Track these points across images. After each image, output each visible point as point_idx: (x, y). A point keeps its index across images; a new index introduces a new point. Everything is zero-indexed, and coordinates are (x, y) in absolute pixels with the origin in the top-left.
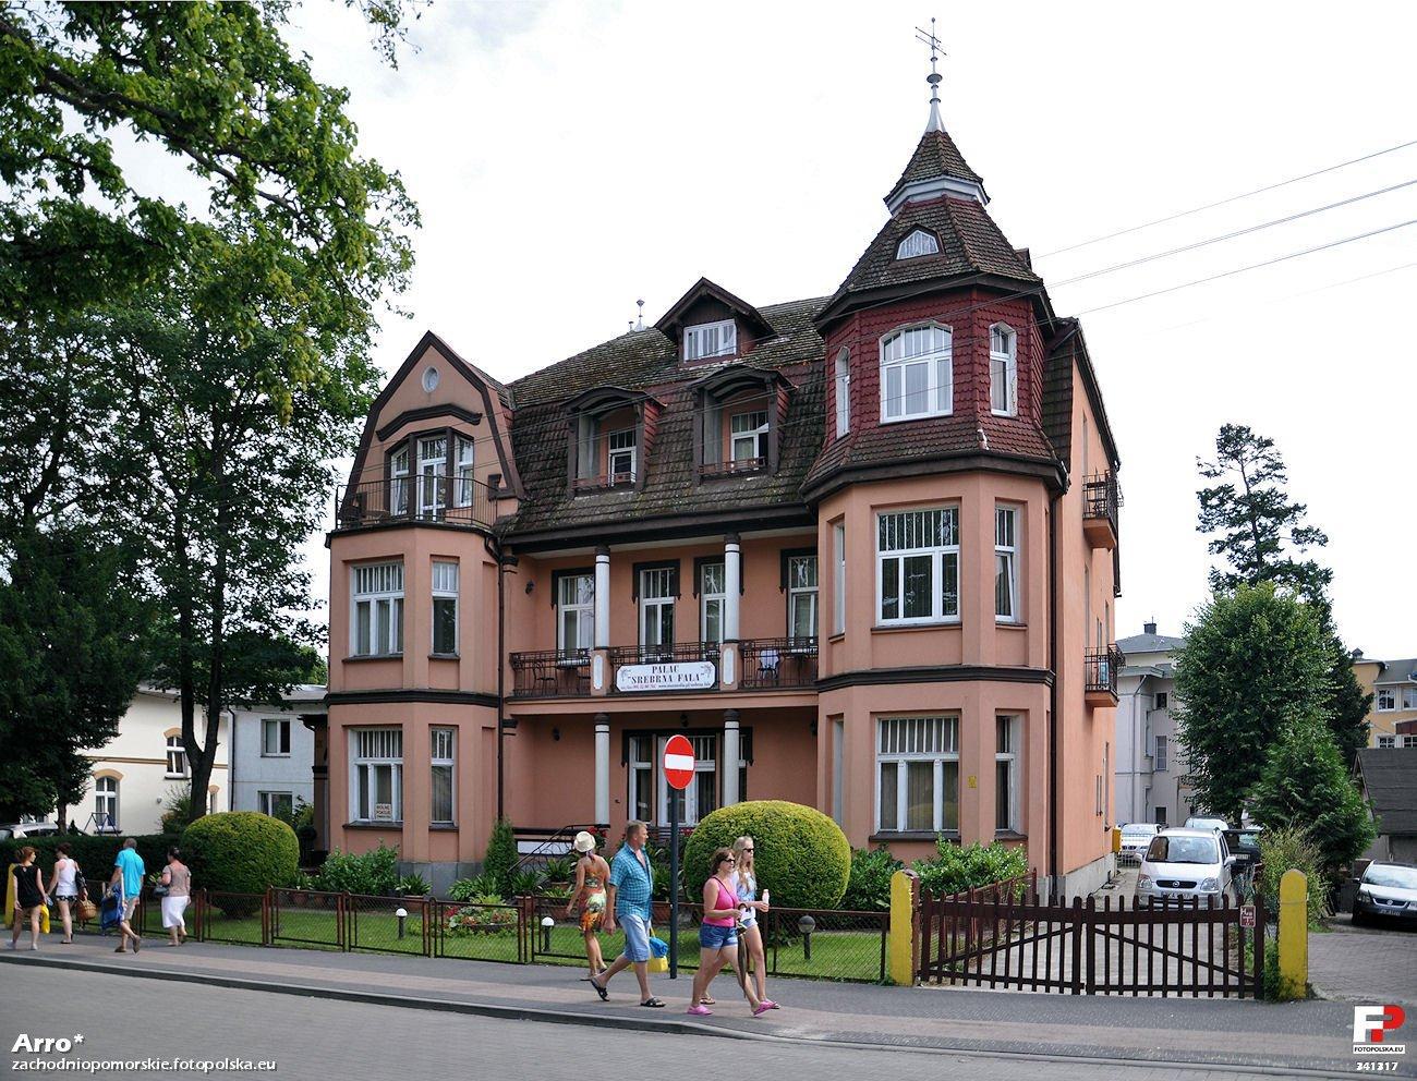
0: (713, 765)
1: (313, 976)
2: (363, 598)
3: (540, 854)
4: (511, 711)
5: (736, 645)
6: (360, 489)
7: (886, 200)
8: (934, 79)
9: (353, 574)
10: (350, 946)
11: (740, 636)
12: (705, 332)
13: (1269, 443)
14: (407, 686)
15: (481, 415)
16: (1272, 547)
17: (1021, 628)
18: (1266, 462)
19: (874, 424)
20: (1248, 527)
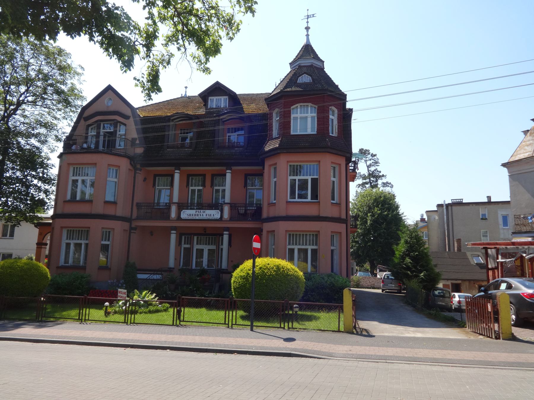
0: (215, 247)
1: (82, 335)
2: (75, 178)
3: (149, 279)
4: (135, 224)
5: (229, 205)
6: (74, 138)
7: (290, 64)
8: (307, 28)
11: (231, 201)
12: (216, 99)
13: (375, 155)
14: (93, 212)
15: (130, 117)
16: (376, 186)
17: (339, 204)
18: (373, 161)
20: (368, 180)
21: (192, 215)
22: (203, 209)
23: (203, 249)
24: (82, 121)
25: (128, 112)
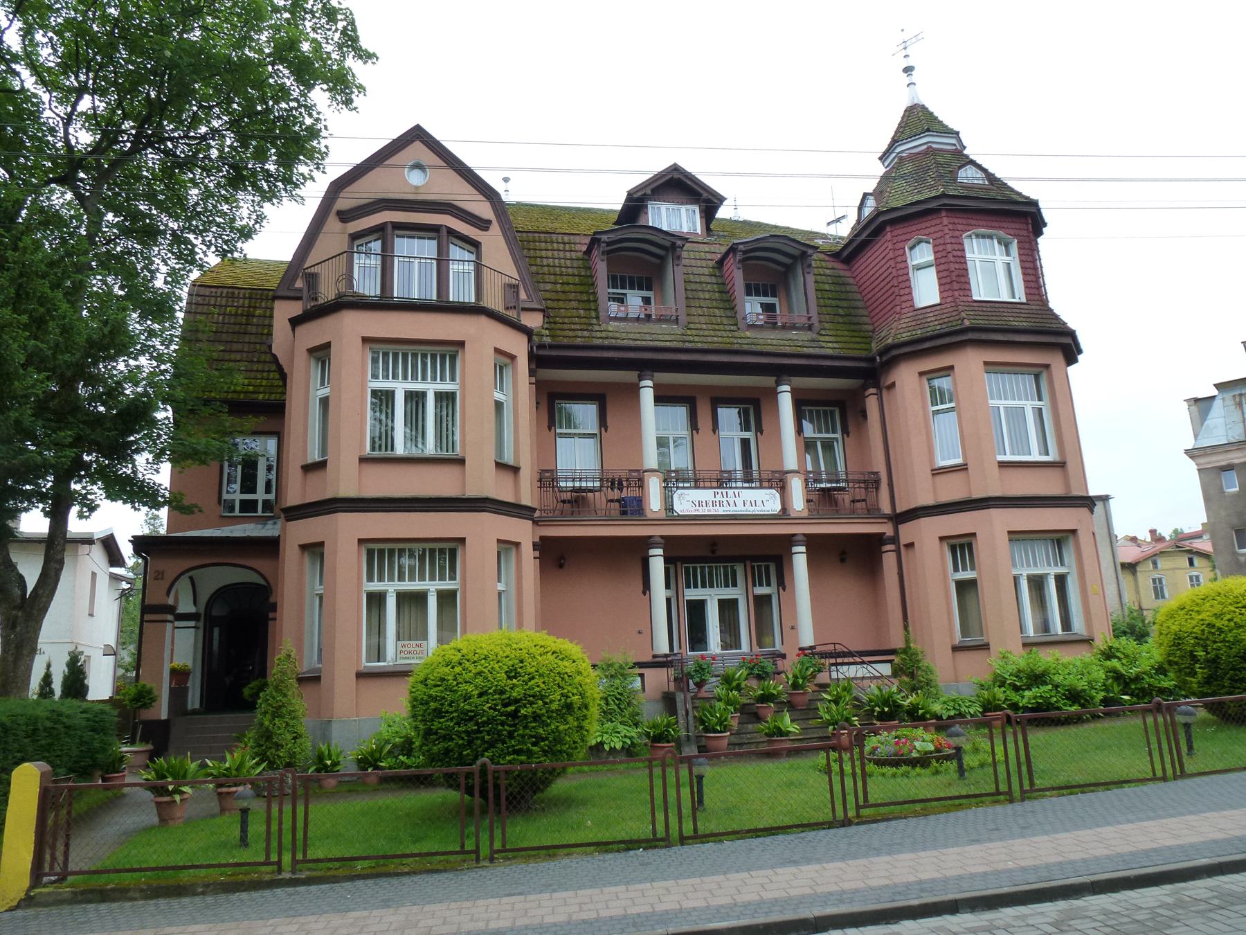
9: (924, 379)
10: (1023, 791)
21: (704, 504)
22: (723, 488)
23: (737, 600)
24: (333, 223)
25: (483, 209)
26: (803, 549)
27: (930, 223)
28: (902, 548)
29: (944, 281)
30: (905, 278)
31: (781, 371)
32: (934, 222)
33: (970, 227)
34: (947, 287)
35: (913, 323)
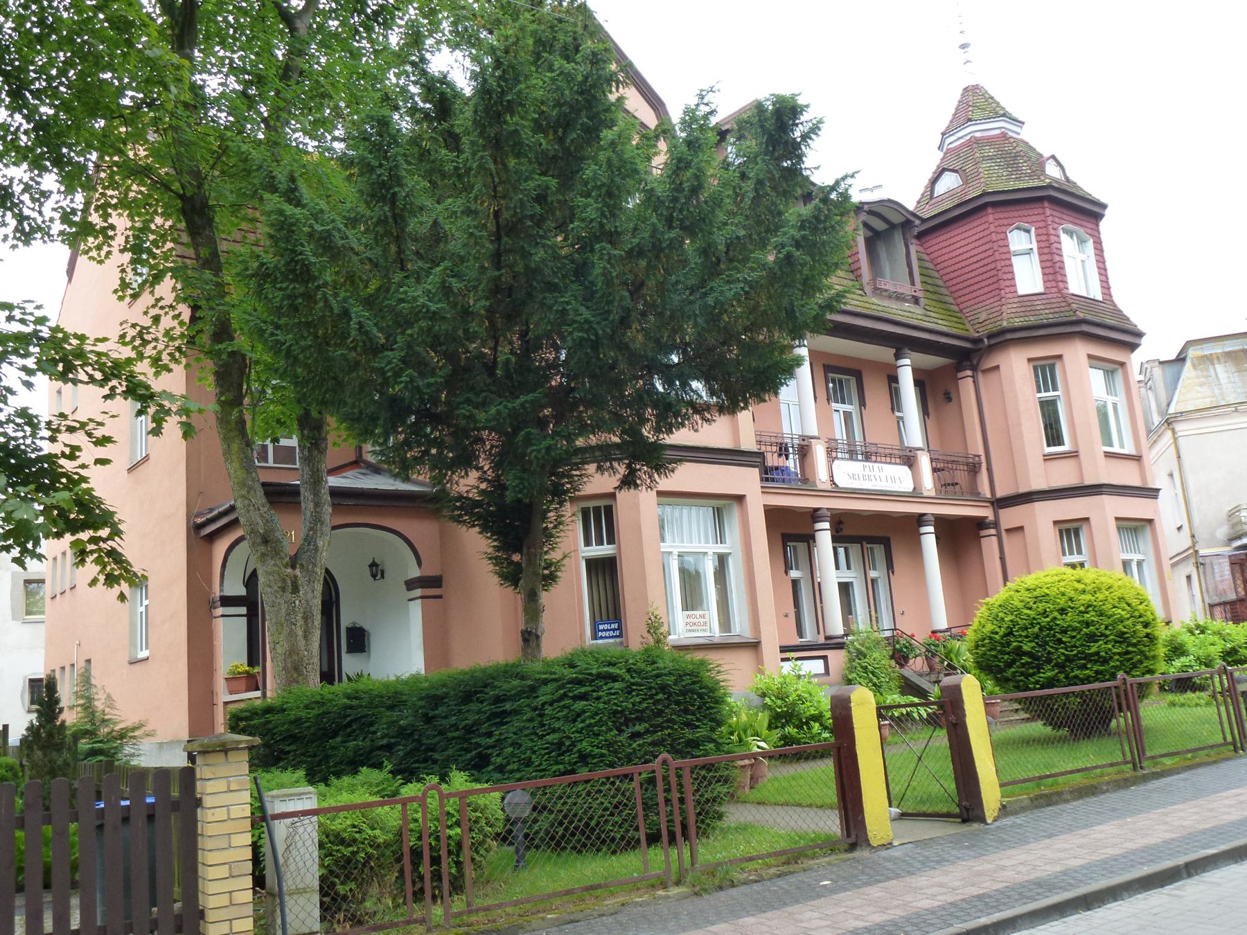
19: (1015, 295)
23: (852, 583)
26: (931, 529)
27: (1035, 210)
28: (1004, 533)
29: (1047, 271)
30: (1007, 263)
31: (901, 344)
32: (1036, 211)
33: (1062, 221)
34: (1051, 277)
35: (1023, 309)
